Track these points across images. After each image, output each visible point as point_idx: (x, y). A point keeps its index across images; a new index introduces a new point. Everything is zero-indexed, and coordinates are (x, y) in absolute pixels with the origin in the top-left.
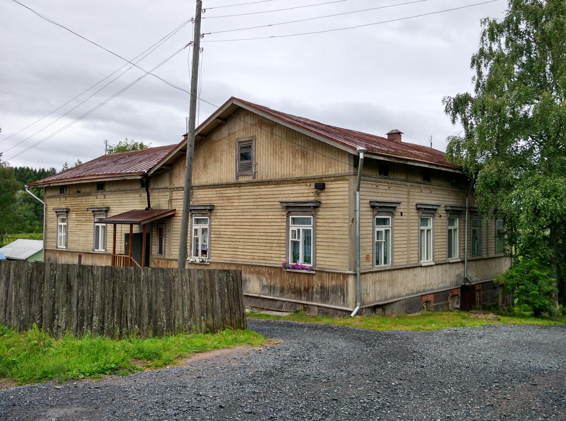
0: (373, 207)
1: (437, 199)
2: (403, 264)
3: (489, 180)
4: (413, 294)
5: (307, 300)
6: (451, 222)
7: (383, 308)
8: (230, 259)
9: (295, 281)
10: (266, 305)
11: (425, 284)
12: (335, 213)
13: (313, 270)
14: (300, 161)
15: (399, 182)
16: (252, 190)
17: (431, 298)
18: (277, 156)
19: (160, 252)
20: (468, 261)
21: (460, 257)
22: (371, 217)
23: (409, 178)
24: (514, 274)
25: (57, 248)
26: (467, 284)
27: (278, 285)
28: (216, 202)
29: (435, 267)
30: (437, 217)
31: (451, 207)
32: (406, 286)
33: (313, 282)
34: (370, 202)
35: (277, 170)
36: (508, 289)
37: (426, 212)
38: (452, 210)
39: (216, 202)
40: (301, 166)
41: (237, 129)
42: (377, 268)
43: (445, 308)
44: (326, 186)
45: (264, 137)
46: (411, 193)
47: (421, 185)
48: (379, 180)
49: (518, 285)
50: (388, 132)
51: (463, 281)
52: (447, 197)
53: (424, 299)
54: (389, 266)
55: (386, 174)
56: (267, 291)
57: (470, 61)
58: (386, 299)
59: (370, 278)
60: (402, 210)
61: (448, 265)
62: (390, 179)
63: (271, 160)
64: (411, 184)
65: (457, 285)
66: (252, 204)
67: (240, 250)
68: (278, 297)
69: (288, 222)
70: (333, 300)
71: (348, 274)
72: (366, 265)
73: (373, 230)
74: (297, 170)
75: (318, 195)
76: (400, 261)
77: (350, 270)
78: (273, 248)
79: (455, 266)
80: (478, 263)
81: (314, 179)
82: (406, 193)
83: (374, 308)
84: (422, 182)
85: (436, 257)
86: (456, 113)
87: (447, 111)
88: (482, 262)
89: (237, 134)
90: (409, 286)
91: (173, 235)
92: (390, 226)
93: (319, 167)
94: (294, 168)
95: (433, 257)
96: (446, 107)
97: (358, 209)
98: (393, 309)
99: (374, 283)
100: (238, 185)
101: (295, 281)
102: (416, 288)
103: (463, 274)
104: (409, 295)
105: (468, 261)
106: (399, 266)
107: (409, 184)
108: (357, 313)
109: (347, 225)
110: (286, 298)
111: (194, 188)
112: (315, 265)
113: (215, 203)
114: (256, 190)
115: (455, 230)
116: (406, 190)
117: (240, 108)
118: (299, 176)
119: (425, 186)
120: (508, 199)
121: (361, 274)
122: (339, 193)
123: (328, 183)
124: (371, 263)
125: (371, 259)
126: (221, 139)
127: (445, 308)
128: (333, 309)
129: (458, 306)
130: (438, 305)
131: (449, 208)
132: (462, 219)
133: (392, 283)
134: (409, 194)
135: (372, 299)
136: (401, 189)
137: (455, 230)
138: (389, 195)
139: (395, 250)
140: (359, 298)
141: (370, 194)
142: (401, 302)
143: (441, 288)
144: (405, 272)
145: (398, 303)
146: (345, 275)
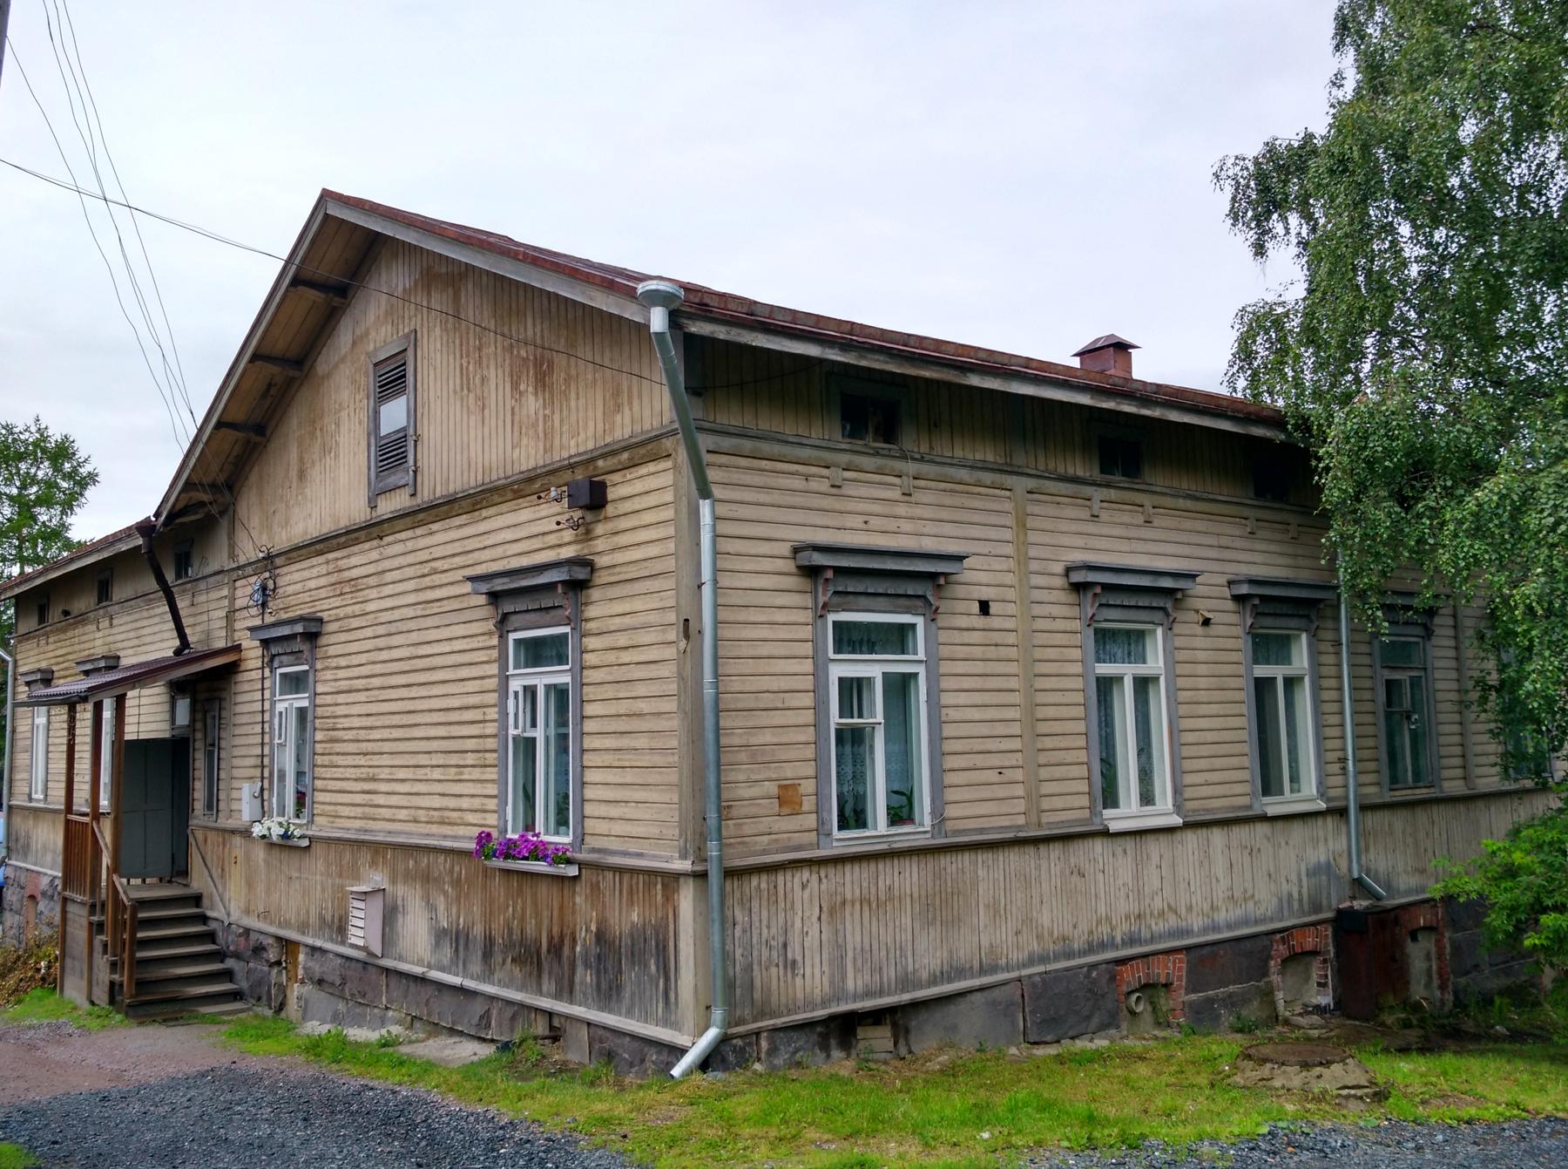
0: (811, 572)
1: (1187, 550)
2: (1005, 822)
3: (1376, 445)
4: (1069, 955)
5: (558, 996)
6: (1268, 646)
7: (895, 1026)
8: (358, 824)
9: (523, 910)
10: (445, 1010)
11: (1134, 908)
12: (638, 605)
13: (569, 862)
14: (532, 404)
15: (963, 474)
16: (410, 545)
17: (1174, 970)
18: (472, 396)
19: (209, 806)
20: (1364, 808)
21: (1322, 794)
22: (807, 616)
23: (1019, 459)
24: (1518, 857)
25: (31, 800)
26: (1360, 904)
27: (478, 931)
28: (325, 605)
29: (1191, 838)
30: (1187, 626)
31: (1252, 582)
32: (1028, 920)
33: (574, 913)
34: (796, 551)
35: (473, 455)
36: (1495, 931)
37: (1123, 605)
38: (1263, 598)
39: (325, 605)
40: (535, 425)
41: (371, 317)
42: (843, 841)
43: (1253, 1011)
44: (612, 494)
45: (438, 330)
46: (1030, 522)
47: (1088, 490)
48: (844, 458)
49: (1539, 908)
50: (1083, 342)
51: (1348, 892)
52: (1239, 543)
53: (1132, 976)
54: (921, 829)
55: (888, 433)
56: (447, 952)
57: (1330, 27)
58: (905, 983)
59: (804, 891)
60: (985, 593)
61: (1262, 829)
62: (904, 457)
63: (471, 420)
64: (1031, 483)
65: (1317, 908)
66: (412, 599)
67: (383, 787)
68: (478, 979)
69: (502, 661)
70: (633, 994)
71: (677, 876)
72: (766, 831)
73: (819, 674)
74: (524, 441)
75: (585, 532)
76: (981, 807)
77: (683, 856)
78: (467, 774)
79: (1298, 831)
80: (1421, 816)
81: (572, 467)
82: (1009, 520)
83: (843, 1029)
84: (1096, 474)
85: (1188, 793)
86: (1269, 213)
87: (1235, 216)
88: (1438, 812)
89: (373, 334)
90: (1045, 920)
91: (238, 741)
92: (921, 655)
93: (585, 422)
94: (516, 434)
95: (1177, 791)
96: (1234, 199)
97: (706, 575)
98: (953, 1028)
99: (834, 910)
100: (373, 530)
101: (523, 910)
102: (1083, 927)
103: (1344, 864)
104: (1043, 959)
105: (1364, 808)
106: (982, 831)
107: (1021, 484)
108: (705, 1065)
109: (670, 652)
110: (500, 983)
111: (278, 561)
112: (581, 838)
113: (328, 607)
114: (422, 543)
115: (1290, 682)
116: (1008, 506)
117: (375, 239)
118: (532, 464)
119: (1113, 494)
120: (1460, 522)
121: (730, 873)
122: (648, 518)
123: (616, 477)
124: (811, 821)
125: (808, 804)
126: (336, 366)
127: (1253, 1011)
128: (635, 1037)
129: (1325, 999)
130: (1210, 1001)
131: (1244, 589)
132: (1323, 634)
133: (940, 910)
134: (1022, 526)
135: (813, 987)
136: (977, 503)
137: (1290, 682)
138: (907, 526)
139: (950, 762)
140: (733, 989)
141: (799, 516)
142: (996, 993)
143: (1229, 927)
144: (1013, 859)
145: (977, 998)
146: (671, 880)
